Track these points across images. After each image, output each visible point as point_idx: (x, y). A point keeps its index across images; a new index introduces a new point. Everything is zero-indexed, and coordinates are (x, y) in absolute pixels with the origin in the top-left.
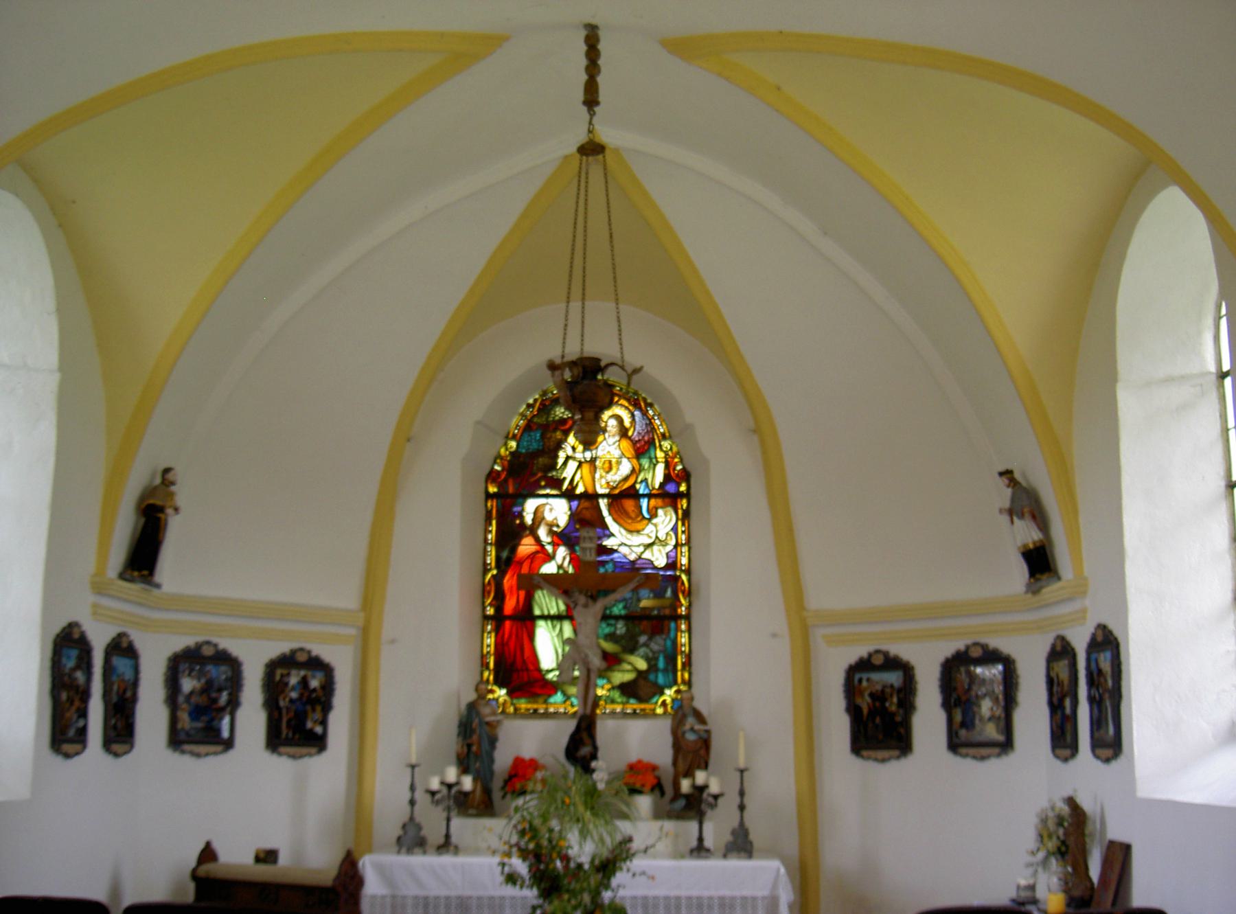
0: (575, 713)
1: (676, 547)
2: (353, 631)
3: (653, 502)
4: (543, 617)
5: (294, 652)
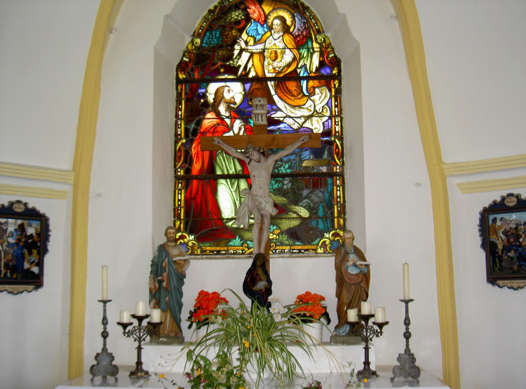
0: (251, 253)
1: (330, 118)
2: (68, 188)
3: (311, 83)
4: (223, 177)
5: (12, 204)
